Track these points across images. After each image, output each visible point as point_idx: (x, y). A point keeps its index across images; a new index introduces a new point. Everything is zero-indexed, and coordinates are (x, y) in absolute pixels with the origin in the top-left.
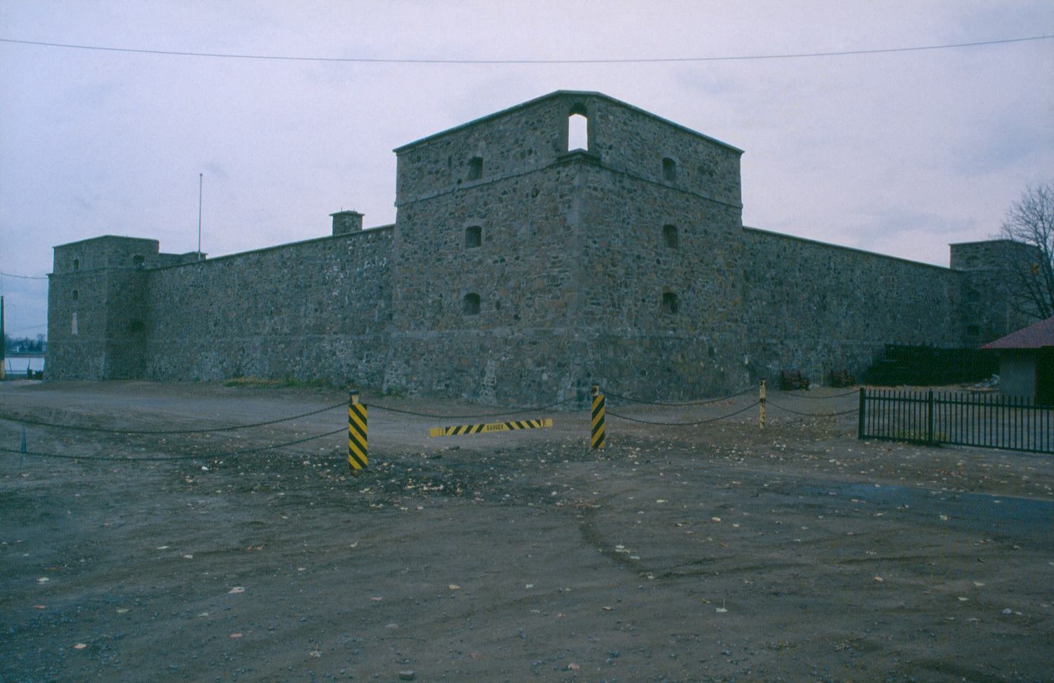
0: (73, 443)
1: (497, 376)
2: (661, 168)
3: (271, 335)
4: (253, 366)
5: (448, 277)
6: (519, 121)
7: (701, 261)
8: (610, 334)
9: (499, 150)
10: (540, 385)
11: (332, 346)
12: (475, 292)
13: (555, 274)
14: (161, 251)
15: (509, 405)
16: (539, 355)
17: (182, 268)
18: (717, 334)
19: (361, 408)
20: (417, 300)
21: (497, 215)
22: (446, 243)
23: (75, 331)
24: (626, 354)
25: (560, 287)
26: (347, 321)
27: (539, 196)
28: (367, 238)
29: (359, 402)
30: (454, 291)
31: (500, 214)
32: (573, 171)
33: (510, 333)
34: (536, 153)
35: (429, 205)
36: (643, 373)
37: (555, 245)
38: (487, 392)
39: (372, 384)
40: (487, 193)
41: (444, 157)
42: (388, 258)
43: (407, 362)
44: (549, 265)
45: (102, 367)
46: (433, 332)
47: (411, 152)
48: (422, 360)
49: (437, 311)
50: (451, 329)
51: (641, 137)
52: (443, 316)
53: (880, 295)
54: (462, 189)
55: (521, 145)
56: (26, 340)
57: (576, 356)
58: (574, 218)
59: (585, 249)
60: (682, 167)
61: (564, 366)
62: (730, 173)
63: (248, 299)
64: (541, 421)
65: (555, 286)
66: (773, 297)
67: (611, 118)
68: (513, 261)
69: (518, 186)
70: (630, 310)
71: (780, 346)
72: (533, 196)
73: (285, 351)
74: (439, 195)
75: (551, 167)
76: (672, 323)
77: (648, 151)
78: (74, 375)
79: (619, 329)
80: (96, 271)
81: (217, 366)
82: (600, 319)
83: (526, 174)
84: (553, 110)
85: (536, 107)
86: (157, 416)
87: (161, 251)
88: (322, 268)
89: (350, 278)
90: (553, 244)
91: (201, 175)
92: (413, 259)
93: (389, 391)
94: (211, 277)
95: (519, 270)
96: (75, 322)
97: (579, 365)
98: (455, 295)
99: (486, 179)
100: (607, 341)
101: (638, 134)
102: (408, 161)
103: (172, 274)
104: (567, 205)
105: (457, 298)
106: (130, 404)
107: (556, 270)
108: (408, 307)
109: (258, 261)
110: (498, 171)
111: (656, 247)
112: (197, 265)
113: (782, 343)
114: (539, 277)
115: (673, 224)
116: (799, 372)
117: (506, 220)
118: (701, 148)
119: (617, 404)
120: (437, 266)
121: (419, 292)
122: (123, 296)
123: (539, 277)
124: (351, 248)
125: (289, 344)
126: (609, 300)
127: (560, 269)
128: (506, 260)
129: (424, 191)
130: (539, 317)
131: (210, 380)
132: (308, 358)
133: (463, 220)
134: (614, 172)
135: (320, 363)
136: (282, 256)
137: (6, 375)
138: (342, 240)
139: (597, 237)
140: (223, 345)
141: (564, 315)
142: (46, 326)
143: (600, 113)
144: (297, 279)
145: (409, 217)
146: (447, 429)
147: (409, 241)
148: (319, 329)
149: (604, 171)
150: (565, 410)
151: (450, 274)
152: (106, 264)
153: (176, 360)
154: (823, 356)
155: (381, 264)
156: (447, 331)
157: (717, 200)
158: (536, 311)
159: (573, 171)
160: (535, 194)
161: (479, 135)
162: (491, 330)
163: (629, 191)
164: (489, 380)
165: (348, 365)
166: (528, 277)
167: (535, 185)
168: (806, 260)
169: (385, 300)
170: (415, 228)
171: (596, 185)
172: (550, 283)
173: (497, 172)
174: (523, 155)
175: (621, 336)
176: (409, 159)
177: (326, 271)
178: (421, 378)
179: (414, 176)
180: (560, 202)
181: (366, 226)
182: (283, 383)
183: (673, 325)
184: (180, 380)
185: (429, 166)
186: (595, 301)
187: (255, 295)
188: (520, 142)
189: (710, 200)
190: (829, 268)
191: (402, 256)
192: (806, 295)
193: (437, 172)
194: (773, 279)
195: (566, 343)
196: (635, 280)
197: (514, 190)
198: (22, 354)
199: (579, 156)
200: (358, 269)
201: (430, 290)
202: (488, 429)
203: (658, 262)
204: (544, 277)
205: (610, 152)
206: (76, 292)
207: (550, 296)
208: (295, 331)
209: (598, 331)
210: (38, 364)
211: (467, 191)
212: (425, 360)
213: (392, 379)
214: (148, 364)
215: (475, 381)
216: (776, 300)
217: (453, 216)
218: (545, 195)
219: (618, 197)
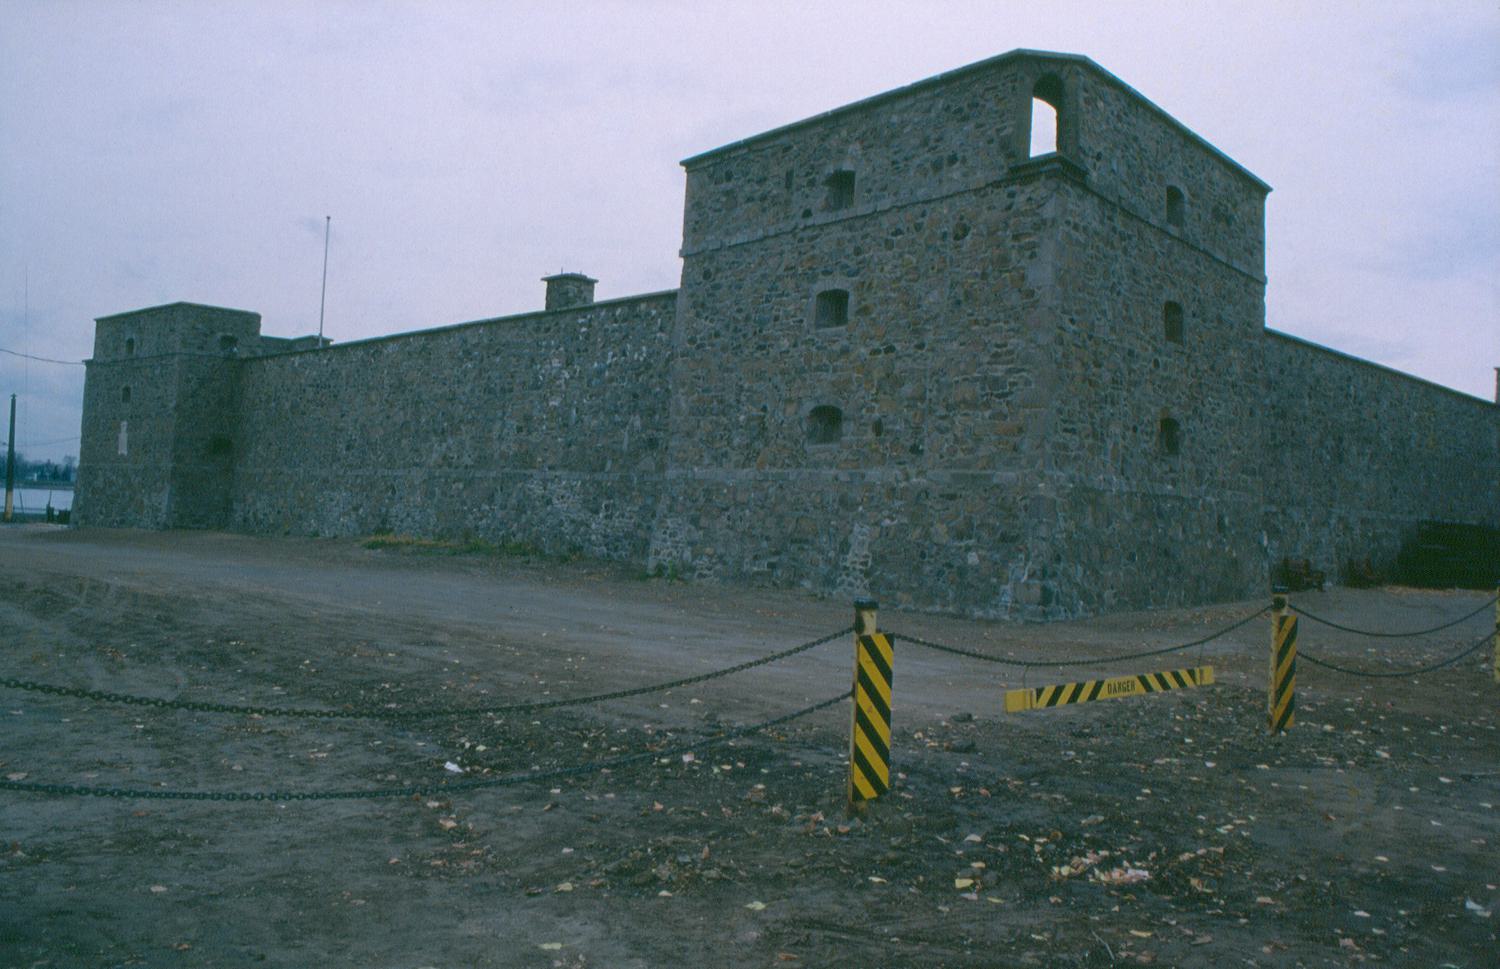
0: (127, 661)
1: (874, 553)
2: (1164, 203)
3: (440, 466)
4: (408, 515)
5: (779, 377)
6: (931, 106)
7: (1212, 368)
8: (1089, 485)
9: (888, 158)
10: (962, 571)
11: (545, 489)
12: (832, 403)
13: (999, 374)
14: (263, 332)
15: (896, 606)
16: (961, 518)
17: (298, 358)
18: (1229, 493)
19: (881, 643)
20: (717, 415)
21: (882, 270)
22: (776, 319)
23: (123, 451)
24: (1109, 523)
25: (1009, 398)
26: (573, 448)
27: (968, 238)
28: (613, 315)
29: (878, 631)
30: (789, 401)
31: (887, 268)
32: (1043, 192)
33: (900, 478)
34: (964, 160)
35: (745, 254)
36: (1131, 558)
37: (1001, 324)
38: (851, 579)
39: (615, 555)
40: (861, 233)
41: (778, 171)
42: (649, 347)
43: (695, 521)
44: (987, 359)
45: (164, 507)
46: (745, 471)
47: (714, 165)
48: (724, 519)
49: (755, 434)
50: (782, 467)
51: (1140, 146)
52: (766, 445)
53: (1412, 441)
54: (813, 225)
55: (934, 148)
56: (48, 465)
57: (1041, 522)
58: (1042, 274)
59: (1059, 331)
60: (1192, 204)
61: (1014, 539)
62: (1252, 223)
63: (403, 408)
64: (1197, 670)
65: (997, 396)
66: (1274, 436)
67: (1101, 104)
68: (911, 351)
69: (925, 220)
70: (1116, 444)
71: (1280, 517)
72: (957, 238)
73: (464, 495)
74: (766, 237)
75: (996, 184)
76: (1171, 470)
77: (1148, 171)
78: (118, 519)
79: (1101, 477)
80: (161, 357)
81: (349, 515)
82: (1077, 458)
83: (943, 199)
84: (1003, 85)
85: (966, 81)
86: (273, 603)
87: (263, 332)
88: (533, 360)
89: (581, 378)
90: (998, 321)
91: (328, 218)
92: (712, 345)
93: (660, 570)
94: (344, 373)
95: (922, 367)
96: (123, 437)
97: (1044, 539)
98: (791, 409)
99: (861, 208)
100: (1084, 497)
101: (1136, 139)
102: (707, 180)
103: (282, 366)
104: (1028, 253)
105: (796, 413)
106: (214, 576)
107: (1000, 367)
108: (698, 427)
109: (424, 348)
110: (886, 193)
111: (1154, 338)
112: (321, 354)
113: (1284, 512)
114: (965, 380)
115: (1177, 300)
116: (1307, 560)
117: (899, 279)
118: (1216, 175)
119: (1096, 612)
120: (758, 359)
121: (721, 402)
122: (199, 397)
123: (965, 380)
124: (584, 329)
125: (469, 483)
126: (1089, 426)
127: (1009, 366)
128: (898, 348)
129: (738, 229)
130: (963, 451)
131: (335, 537)
132: (503, 507)
133: (813, 279)
134: (1103, 200)
135: (524, 516)
136: (465, 341)
137: (14, 515)
138: (569, 317)
139: (1077, 312)
140: (359, 481)
141: (1015, 449)
142: (79, 440)
143: (1086, 95)
144: (489, 378)
145: (707, 275)
146: (1039, 692)
147: (705, 315)
148: (525, 459)
149: (1089, 196)
150: (1016, 620)
151: (783, 372)
152: (178, 347)
153: (281, 502)
154: (1338, 536)
155: (636, 356)
156: (775, 470)
157: (1236, 266)
158: (956, 440)
159: (1043, 192)
160: (960, 233)
161: (849, 134)
162: (863, 471)
163: (1122, 238)
164: (856, 559)
165: (573, 521)
166: (943, 380)
167: (962, 218)
168: (1318, 380)
169: (641, 417)
170: (718, 293)
171: (1077, 220)
172: (988, 391)
173: (884, 196)
174: (937, 166)
175: (1104, 491)
176: (711, 177)
177: (539, 366)
178: (721, 550)
179: (718, 206)
180: (1013, 247)
181: (600, 295)
182: (459, 547)
183: (1172, 475)
184: (287, 533)
185: (747, 189)
186: (1070, 427)
187: (417, 403)
188: (932, 144)
189: (1228, 266)
190: (1348, 396)
191: (692, 341)
192: (1316, 436)
193: (763, 198)
194: (1273, 407)
195: (1019, 498)
196: (1125, 393)
197: (918, 227)
198: (40, 484)
199: (1057, 165)
200: (596, 365)
201: (743, 398)
202: (1109, 692)
203: (1156, 363)
204: (976, 379)
205: (1098, 164)
206: (127, 390)
207: (987, 414)
208: (482, 461)
209: (1071, 479)
210: (63, 500)
211: (822, 229)
212: (729, 518)
213: (664, 549)
214: (235, 505)
215: (828, 561)
216: (1277, 442)
217: (791, 272)
218: (982, 235)
219: (1106, 245)
